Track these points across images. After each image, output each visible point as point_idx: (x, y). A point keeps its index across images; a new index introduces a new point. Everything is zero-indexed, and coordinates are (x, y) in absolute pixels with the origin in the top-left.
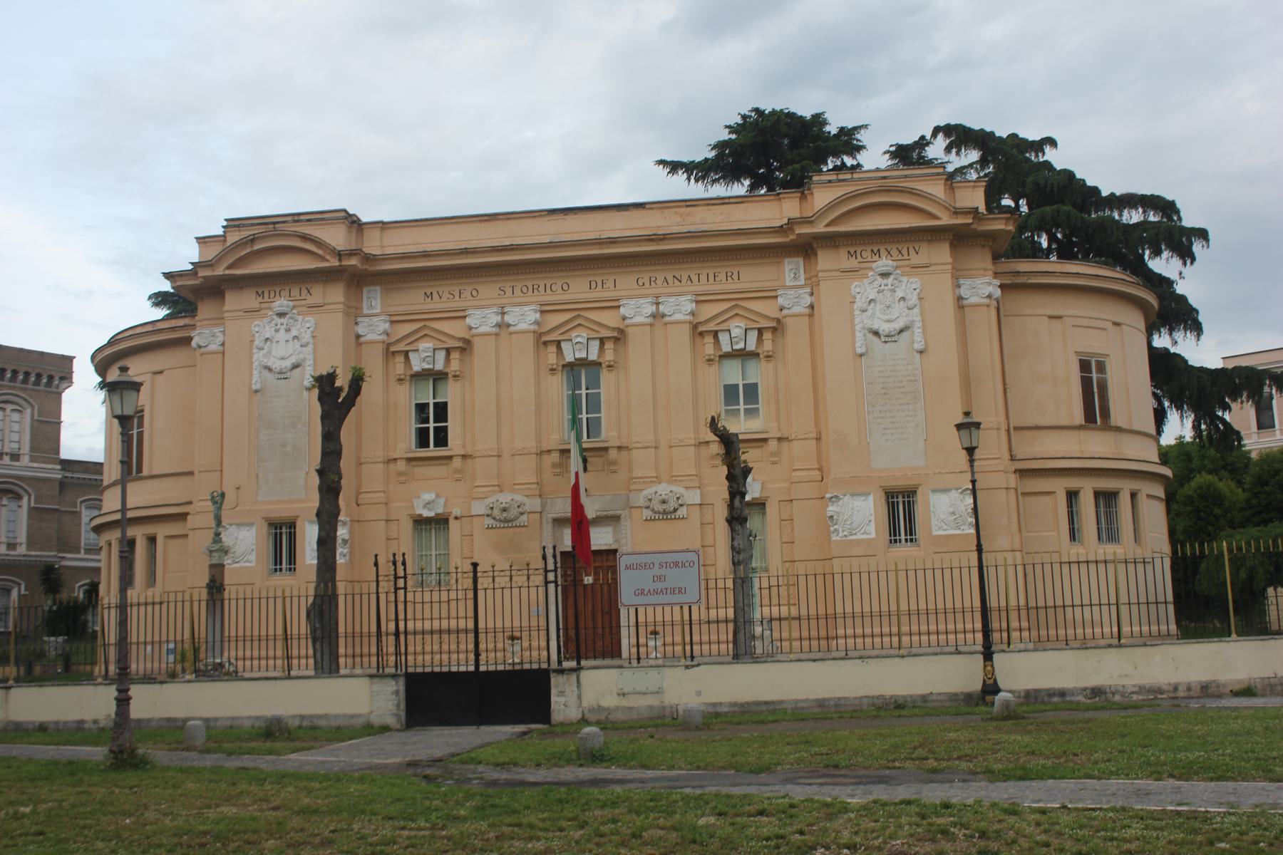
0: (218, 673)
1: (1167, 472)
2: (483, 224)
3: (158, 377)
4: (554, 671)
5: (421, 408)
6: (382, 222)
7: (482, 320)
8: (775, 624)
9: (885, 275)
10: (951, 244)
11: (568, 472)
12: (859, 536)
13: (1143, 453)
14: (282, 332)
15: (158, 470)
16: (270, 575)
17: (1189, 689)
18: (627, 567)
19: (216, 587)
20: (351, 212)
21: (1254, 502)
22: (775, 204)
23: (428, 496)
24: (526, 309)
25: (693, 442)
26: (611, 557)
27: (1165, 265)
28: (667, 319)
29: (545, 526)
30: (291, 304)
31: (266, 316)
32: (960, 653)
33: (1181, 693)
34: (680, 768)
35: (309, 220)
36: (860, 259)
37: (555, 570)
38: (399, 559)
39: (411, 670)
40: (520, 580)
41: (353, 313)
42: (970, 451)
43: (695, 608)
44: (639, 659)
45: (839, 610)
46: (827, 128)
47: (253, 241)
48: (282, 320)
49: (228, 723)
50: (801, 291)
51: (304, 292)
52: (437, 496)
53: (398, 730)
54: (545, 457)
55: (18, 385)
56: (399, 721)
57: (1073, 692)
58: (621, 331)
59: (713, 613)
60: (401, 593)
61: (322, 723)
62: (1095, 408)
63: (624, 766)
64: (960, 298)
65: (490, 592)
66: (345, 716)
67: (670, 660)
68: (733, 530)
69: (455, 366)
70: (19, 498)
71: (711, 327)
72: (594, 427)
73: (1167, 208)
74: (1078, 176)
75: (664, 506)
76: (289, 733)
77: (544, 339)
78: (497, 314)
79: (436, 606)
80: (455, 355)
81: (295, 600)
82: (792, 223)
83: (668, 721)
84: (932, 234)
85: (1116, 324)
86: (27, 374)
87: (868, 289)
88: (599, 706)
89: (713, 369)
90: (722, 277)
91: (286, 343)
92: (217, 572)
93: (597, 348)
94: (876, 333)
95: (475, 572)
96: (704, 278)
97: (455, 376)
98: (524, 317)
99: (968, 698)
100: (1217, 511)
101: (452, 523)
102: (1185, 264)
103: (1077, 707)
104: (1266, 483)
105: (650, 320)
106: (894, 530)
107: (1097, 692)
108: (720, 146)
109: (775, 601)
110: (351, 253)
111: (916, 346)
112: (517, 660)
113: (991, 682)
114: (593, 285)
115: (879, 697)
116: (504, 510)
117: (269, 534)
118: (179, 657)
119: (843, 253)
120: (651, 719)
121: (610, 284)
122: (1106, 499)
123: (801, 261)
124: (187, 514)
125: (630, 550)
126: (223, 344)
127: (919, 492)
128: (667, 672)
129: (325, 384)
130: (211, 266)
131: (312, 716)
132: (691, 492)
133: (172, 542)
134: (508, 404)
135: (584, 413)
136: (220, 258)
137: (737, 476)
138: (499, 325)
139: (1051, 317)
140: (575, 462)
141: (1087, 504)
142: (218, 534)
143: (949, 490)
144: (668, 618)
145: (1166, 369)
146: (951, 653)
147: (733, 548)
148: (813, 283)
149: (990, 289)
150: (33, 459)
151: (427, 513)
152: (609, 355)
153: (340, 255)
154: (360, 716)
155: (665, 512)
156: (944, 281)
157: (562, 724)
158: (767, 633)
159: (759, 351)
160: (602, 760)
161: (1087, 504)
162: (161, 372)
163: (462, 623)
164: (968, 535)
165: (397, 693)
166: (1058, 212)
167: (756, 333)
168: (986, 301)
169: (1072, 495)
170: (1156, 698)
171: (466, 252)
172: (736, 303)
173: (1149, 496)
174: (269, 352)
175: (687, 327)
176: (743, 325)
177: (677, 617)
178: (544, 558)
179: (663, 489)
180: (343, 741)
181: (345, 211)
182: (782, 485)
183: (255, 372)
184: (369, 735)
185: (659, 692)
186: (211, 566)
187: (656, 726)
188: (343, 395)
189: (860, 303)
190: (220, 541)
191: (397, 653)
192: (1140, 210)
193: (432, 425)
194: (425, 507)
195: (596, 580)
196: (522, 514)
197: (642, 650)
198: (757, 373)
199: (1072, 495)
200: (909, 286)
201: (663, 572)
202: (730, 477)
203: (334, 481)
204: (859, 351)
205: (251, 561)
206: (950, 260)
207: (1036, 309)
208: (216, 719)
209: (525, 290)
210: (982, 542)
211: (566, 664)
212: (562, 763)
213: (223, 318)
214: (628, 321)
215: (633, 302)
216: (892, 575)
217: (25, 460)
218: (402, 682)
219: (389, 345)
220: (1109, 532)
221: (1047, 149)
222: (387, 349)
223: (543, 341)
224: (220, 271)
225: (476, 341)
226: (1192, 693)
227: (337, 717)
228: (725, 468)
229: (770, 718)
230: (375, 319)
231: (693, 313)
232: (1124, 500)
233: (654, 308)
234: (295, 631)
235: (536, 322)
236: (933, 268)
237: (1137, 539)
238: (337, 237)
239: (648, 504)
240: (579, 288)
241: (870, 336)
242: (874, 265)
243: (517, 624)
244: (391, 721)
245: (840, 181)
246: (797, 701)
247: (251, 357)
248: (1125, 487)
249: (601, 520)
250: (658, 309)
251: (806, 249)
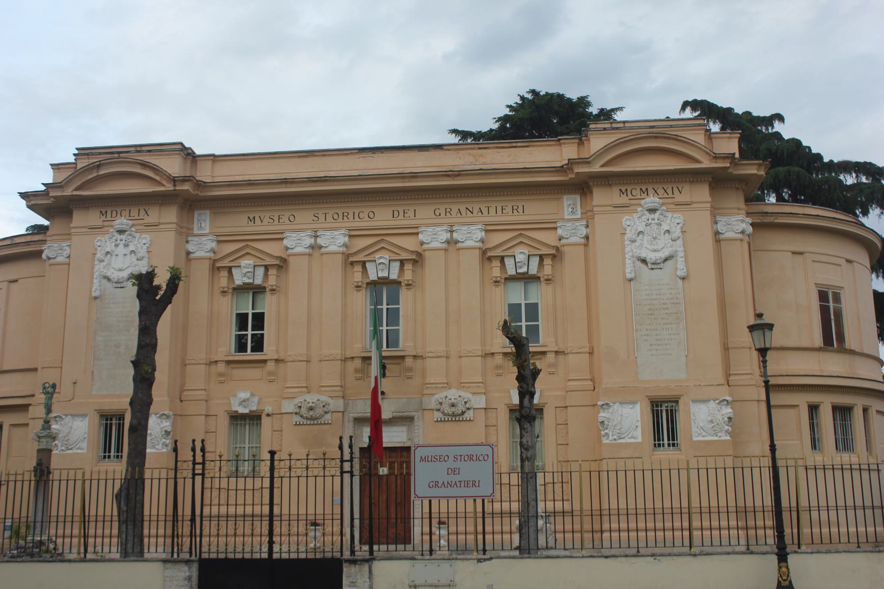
3: (13, 285)
4: (347, 561)
5: (514, 309)
6: (214, 155)
7: (297, 242)
9: (652, 211)
10: (710, 186)
14: (121, 246)
19: (42, 471)
20: (187, 146)
22: (558, 148)
23: (243, 395)
24: (336, 233)
25: (480, 353)
26: (405, 454)
29: (346, 424)
31: (107, 232)
32: (752, 553)
35: (149, 151)
36: (630, 196)
37: (351, 460)
39: (205, 556)
40: (316, 467)
41: (185, 232)
42: (763, 352)
46: (590, 110)
51: (142, 212)
52: (252, 395)
58: (419, 255)
59: (497, 506)
60: (198, 479)
62: (832, 334)
64: (717, 233)
65: (286, 481)
67: (459, 551)
69: (272, 281)
71: (498, 252)
72: (392, 341)
74: (804, 144)
75: (453, 409)
77: (351, 259)
78: (311, 236)
80: (272, 272)
84: (693, 176)
87: (637, 223)
89: (499, 291)
90: (509, 210)
91: (122, 252)
92: (44, 455)
93: (398, 268)
94: (644, 261)
95: (272, 460)
96: (492, 210)
97: (272, 290)
98: (334, 240)
101: (265, 420)
105: (444, 246)
108: (504, 119)
109: (550, 496)
110: (184, 180)
111: (680, 273)
113: (787, 583)
116: (311, 409)
117: (101, 424)
119: (616, 190)
121: (410, 213)
122: (842, 412)
123: (578, 197)
124: (29, 405)
126: (69, 257)
127: (681, 402)
128: (460, 565)
129: (144, 282)
130: (61, 187)
132: (478, 398)
133: (16, 430)
134: (318, 316)
137: (527, 379)
138: (312, 247)
139: (794, 253)
140: (374, 369)
141: (826, 416)
142: (47, 422)
143: (708, 401)
147: (522, 445)
148: (588, 217)
149: (744, 226)
151: (242, 410)
152: (408, 275)
155: (454, 415)
156: (706, 216)
159: (540, 275)
161: (826, 416)
165: (189, 579)
167: (537, 259)
168: (740, 236)
169: (813, 409)
171: (285, 182)
172: (521, 232)
173: (878, 412)
174: (109, 264)
175: (477, 253)
176: (526, 252)
178: (341, 448)
179: (453, 394)
181: (181, 144)
183: (95, 281)
186: (39, 451)
188: (162, 293)
189: (630, 234)
190: (49, 428)
191: (192, 535)
193: (250, 332)
194: (240, 404)
195: (391, 468)
196: (326, 413)
198: (538, 294)
199: (813, 409)
200: (673, 221)
202: (520, 378)
203: (147, 373)
204: (629, 276)
206: (709, 199)
207: (782, 245)
209: (336, 216)
211: (359, 555)
213: (70, 234)
214: (425, 246)
216: (683, 474)
218: (195, 568)
219: (215, 261)
220: (844, 443)
222: (213, 265)
223: (350, 261)
224: (68, 192)
225: (291, 260)
228: (515, 369)
230: (204, 238)
231: (482, 241)
232: (858, 414)
233: (449, 235)
235: (345, 245)
238: (173, 166)
239: (439, 407)
240: (383, 216)
241: (639, 264)
242: (643, 202)
245: (614, 129)
247: (93, 268)
249: (394, 421)
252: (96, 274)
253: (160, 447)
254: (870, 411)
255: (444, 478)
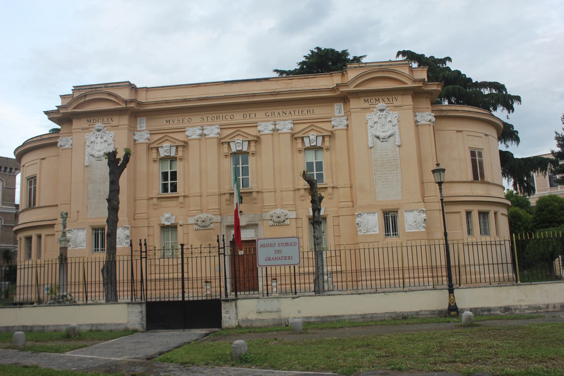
0: (61, 301)
2: (195, 88)
3: (43, 161)
4: (224, 300)
6: (146, 88)
7: (193, 133)
9: (382, 110)
10: (412, 96)
13: (498, 195)
14: (99, 138)
16: (93, 253)
17: (554, 307)
19: (63, 259)
23: (167, 215)
24: (213, 127)
26: (254, 243)
27: (500, 113)
29: (222, 229)
32: (435, 289)
33: (550, 309)
36: (370, 103)
39: (149, 300)
41: (133, 130)
43: (297, 267)
44: (268, 294)
46: (349, 57)
47: (85, 96)
48: (99, 133)
49: (54, 328)
50: (342, 118)
51: (110, 120)
52: (172, 215)
53: (142, 332)
54: (223, 197)
56: (142, 327)
57: (494, 309)
58: (258, 137)
59: (302, 270)
60: (144, 260)
61: (103, 328)
62: (478, 174)
64: (416, 122)
65: (190, 259)
66: (115, 324)
67: (283, 294)
69: (180, 154)
71: (300, 135)
72: (246, 183)
75: (279, 219)
76: (80, 335)
78: (200, 129)
80: (180, 149)
82: (338, 86)
83: (282, 328)
84: (403, 91)
85: (486, 135)
89: (301, 155)
90: (305, 112)
91: (100, 141)
92: (64, 250)
94: (378, 138)
96: (297, 113)
97: (180, 159)
98: (213, 131)
100: (519, 223)
101: (179, 229)
103: (498, 318)
104: (543, 211)
105: (271, 132)
108: (303, 63)
110: (131, 101)
113: (453, 304)
115: (393, 313)
116: (203, 221)
119: (362, 100)
120: (274, 325)
121: (253, 115)
122: (483, 215)
123: (342, 104)
126: (72, 145)
127: (399, 212)
129: (111, 157)
130: (66, 107)
131: (97, 324)
132: (291, 212)
134: (205, 172)
135: (240, 172)
136: (70, 104)
137: (316, 202)
139: (457, 131)
140: (236, 199)
141: (475, 217)
144: (283, 272)
146: (431, 290)
147: (314, 237)
148: (348, 114)
151: (167, 223)
152: (253, 149)
153: (126, 102)
154: (122, 324)
155: (279, 222)
159: (323, 146)
160: (246, 362)
161: (475, 217)
162: (44, 159)
165: (141, 312)
166: (454, 88)
168: (428, 123)
169: (468, 213)
170: (537, 312)
171: (185, 100)
173: (502, 214)
174: (93, 148)
176: (315, 134)
177: (288, 271)
178: (218, 241)
179: (278, 211)
180: (107, 340)
181: (129, 82)
182: (334, 209)
185: (278, 311)
186: (61, 248)
187: (277, 331)
188: (121, 162)
189: (370, 123)
192: (489, 89)
193: (169, 182)
194: (166, 220)
196: (211, 223)
198: (322, 157)
199: (468, 213)
200: (393, 116)
202: (313, 202)
203: (115, 205)
204: (370, 146)
205: (84, 246)
206: (412, 104)
207: (451, 126)
208: (48, 326)
209: (213, 118)
211: (230, 297)
212: (221, 362)
215: (263, 124)
218: (144, 306)
219: (149, 144)
220: (485, 231)
222: (149, 146)
223: (221, 142)
224: (70, 110)
225: (190, 142)
226: (556, 309)
227: (110, 325)
228: (310, 197)
230: (143, 133)
231: (292, 129)
232: (492, 215)
233: (274, 126)
235: (218, 134)
236: (404, 107)
237: (497, 234)
238: (125, 94)
239: (271, 218)
240: (238, 117)
241: (375, 139)
242: (377, 106)
243: (208, 275)
244: (138, 327)
245: (360, 67)
246: (351, 315)
248: (492, 209)
249: (247, 227)
250: (275, 127)
251: (344, 98)
252: (87, 154)
253: (124, 244)
254: (498, 214)
255: (274, 255)
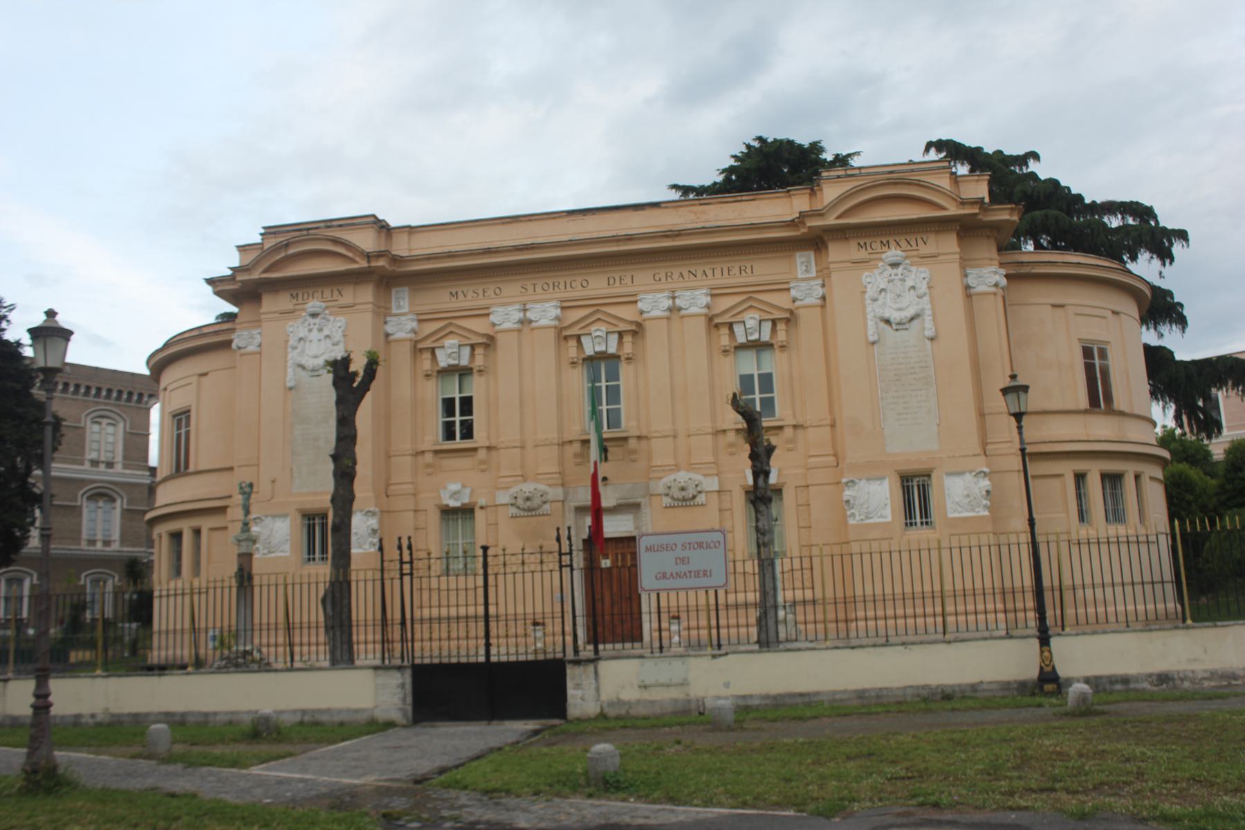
1: (1166, 454)
2: (509, 226)
3: (204, 379)
6: (409, 227)
7: (505, 316)
8: (800, 609)
9: (895, 265)
11: (589, 461)
12: (876, 520)
13: (1142, 437)
14: (315, 332)
15: (201, 468)
18: (647, 549)
19: (244, 578)
20: (380, 217)
21: (1229, 487)
23: (454, 487)
24: (547, 305)
25: (710, 431)
27: (1145, 267)
28: (683, 312)
30: (324, 305)
31: (300, 317)
32: (1011, 637)
34: (721, 805)
35: (340, 226)
38: (405, 543)
39: (418, 661)
41: (382, 312)
43: (721, 593)
44: (661, 648)
45: (859, 592)
49: (227, 718)
50: (812, 283)
51: (336, 293)
52: (464, 486)
53: (404, 726)
55: (112, 401)
56: (405, 715)
57: (1137, 679)
58: (639, 325)
61: (324, 718)
62: (1099, 395)
63: (647, 798)
64: (968, 287)
65: (501, 578)
66: (349, 710)
67: (694, 647)
68: (757, 511)
69: (479, 361)
70: (113, 500)
71: (726, 318)
72: (614, 421)
73: (1143, 212)
74: (1063, 184)
75: (683, 493)
76: (279, 733)
78: (519, 310)
79: (462, 593)
81: (297, 587)
82: (803, 215)
83: (692, 718)
86: (120, 392)
88: (619, 700)
89: (729, 360)
90: (736, 271)
91: (316, 336)
92: (245, 560)
94: (888, 322)
96: (718, 272)
97: (480, 371)
98: (545, 313)
99: (1022, 687)
100: (1189, 497)
101: (479, 514)
102: (1164, 264)
103: (1142, 696)
105: (666, 314)
106: (909, 513)
107: (1163, 678)
108: (729, 171)
110: (380, 255)
112: (539, 645)
113: (1049, 669)
114: (612, 281)
115: (924, 687)
116: (528, 499)
118: (217, 643)
119: (853, 244)
121: (627, 280)
122: (1112, 480)
123: (812, 254)
125: (650, 531)
126: (260, 346)
127: (934, 476)
128: (692, 661)
129: (340, 369)
131: (313, 711)
133: (215, 534)
134: (530, 398)
136: (256, 263)
137: (760, 457)
138: (521, 322)
139: (1054, 306)
141: (1094, 485)
142: (246, 524)
145: (1157, 359)
146: (1001, 638)
149: (997, 278)
150: (125, 467)
151: (453, 504)
152: (628, 348)
154: (363, 710)
155: (684, 499)
156: (952, 269)
157: (579, 720)
158: (790, 617)
159: (773, 342)
162: (206, 374)
163: (471, 611)
164: (982, 517)
165: (403, 686)
168: (993, 289)
169: (1080, 478)
170: (1229, 685)
172: (750, 296)
173: (1152, 478)
174: (303, 351)
175: (703, 320)
176: (757, 316)
177: (702, 601)
179: (682, 477)
180: (334, 742)
181: (374, 216)
184: (368, 734)
185: (684, 684)
186: (240, 555)
187: (681, 724)
188: (359, 379)
189: (871, 292)
195: (615, 561)
196: (545, 503)
197: (665, 634)
198: (772, 363)
199: (1080, 478)
200: (918, 276)
201: (687, 553)
202: (753, 456)
204: (871, 339)
206: (958, 250)
207: (1041, 297)
208: (215, 714)
209: (546, 287)
210: (1035, 516)
211: (583, 655)
212: (566, 790)
213: (259, 321)
217: (119, 467)
218: (408, 675)
219: (416, 342)
220: (1115, 514)
221: (1031, 162)
222: (415, 347)
223: (563, 335)
224: (256, 275)
225: (499, 337)
227: (340, 711)
228: (747, 447)
229: (808, 714)
230: (403, 318)
231: (708, 307)
232: (1129, 481)
234: (297, 620)
235: (557, 318)
236: (941, 258)
238: (366, 241)
240: (597, 284)
241: (882, 325)
242: (884, 256)
244: (396, 716)
245: (849, 176)
246: (835, 692)
247: (286, 356)
251: (817, 242)
252: (290, 363)
253: (367, 546)
